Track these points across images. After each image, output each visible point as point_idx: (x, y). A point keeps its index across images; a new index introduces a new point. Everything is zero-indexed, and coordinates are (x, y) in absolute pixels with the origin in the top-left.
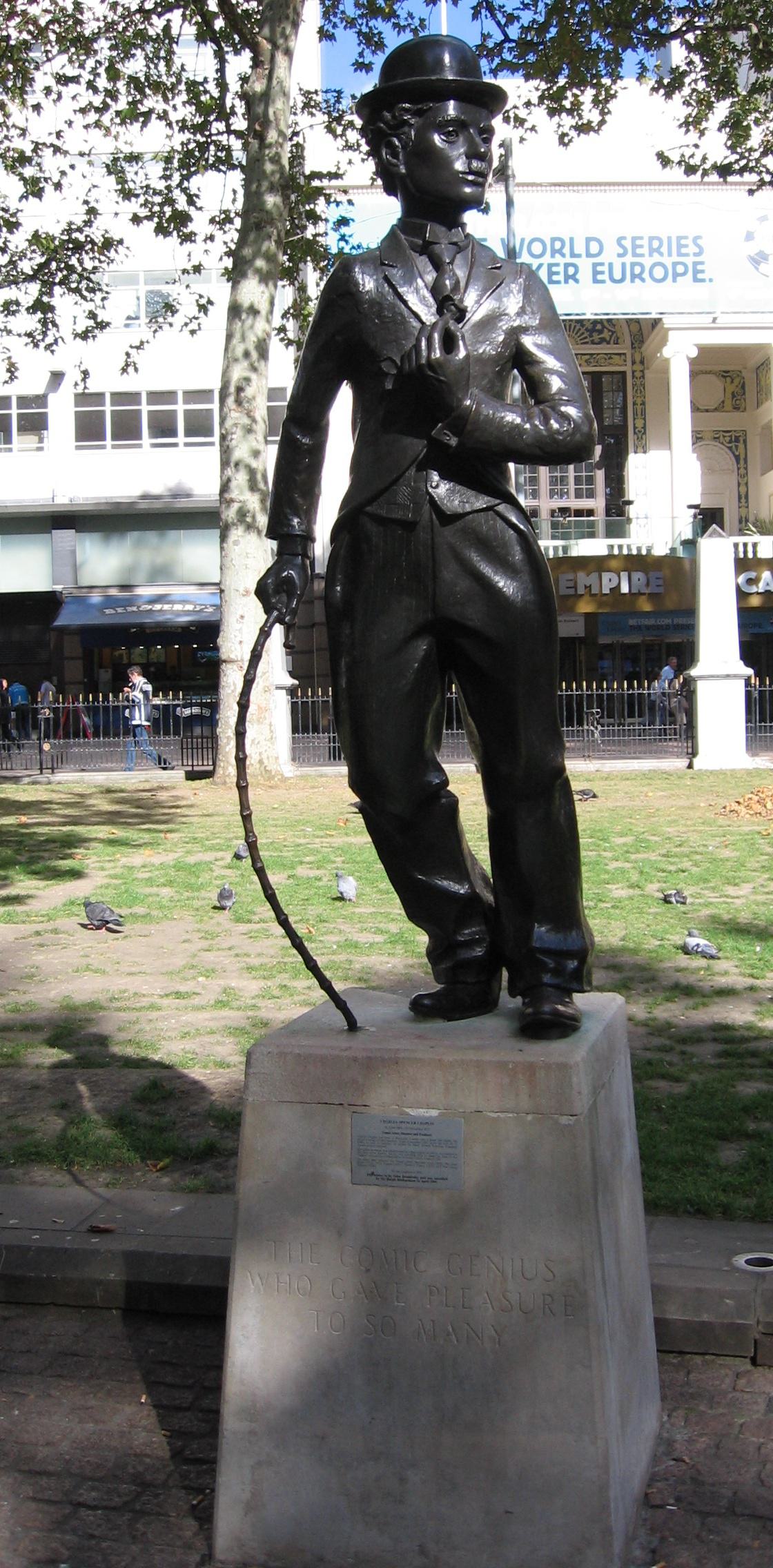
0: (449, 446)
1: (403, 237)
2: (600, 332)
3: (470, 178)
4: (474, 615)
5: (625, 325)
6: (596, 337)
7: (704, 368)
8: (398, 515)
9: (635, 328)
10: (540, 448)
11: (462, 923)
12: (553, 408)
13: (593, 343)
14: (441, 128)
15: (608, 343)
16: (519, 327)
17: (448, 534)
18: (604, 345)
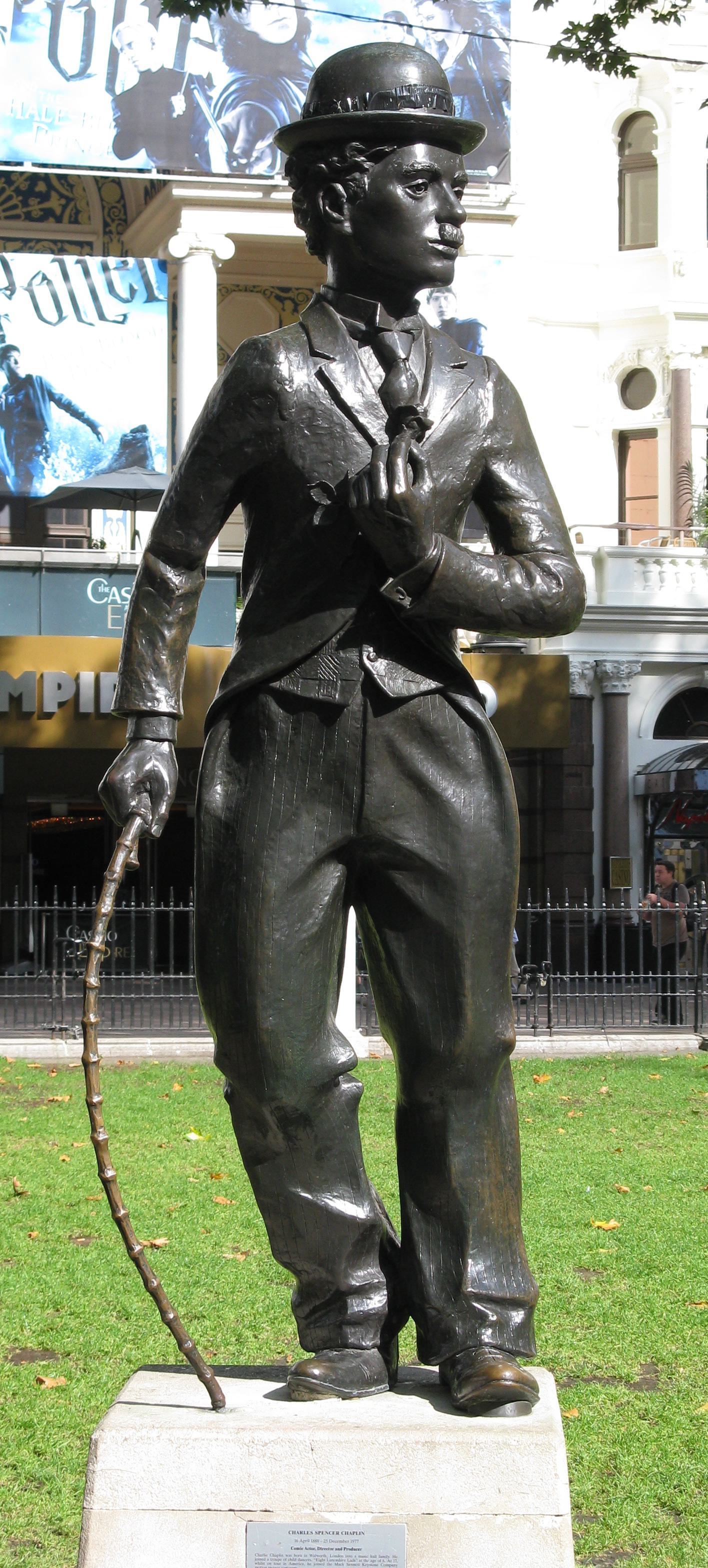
0: (401, 607)
1: (339, 316)
2: (44, 197)
3: (440, 247)
4: (413, 837)
5: (93, 189)
6: (35, 207)
7: (243, 280)
8: (320, 694)
9: (111, 195)
10: (521, 616)
11: (357, 1258)
12: (538, 564)
13: (29, 217)
14: (407, 177)
15: (59, 220)
16: (490, 448)
17: (387, 726)
18: (51, 224)
